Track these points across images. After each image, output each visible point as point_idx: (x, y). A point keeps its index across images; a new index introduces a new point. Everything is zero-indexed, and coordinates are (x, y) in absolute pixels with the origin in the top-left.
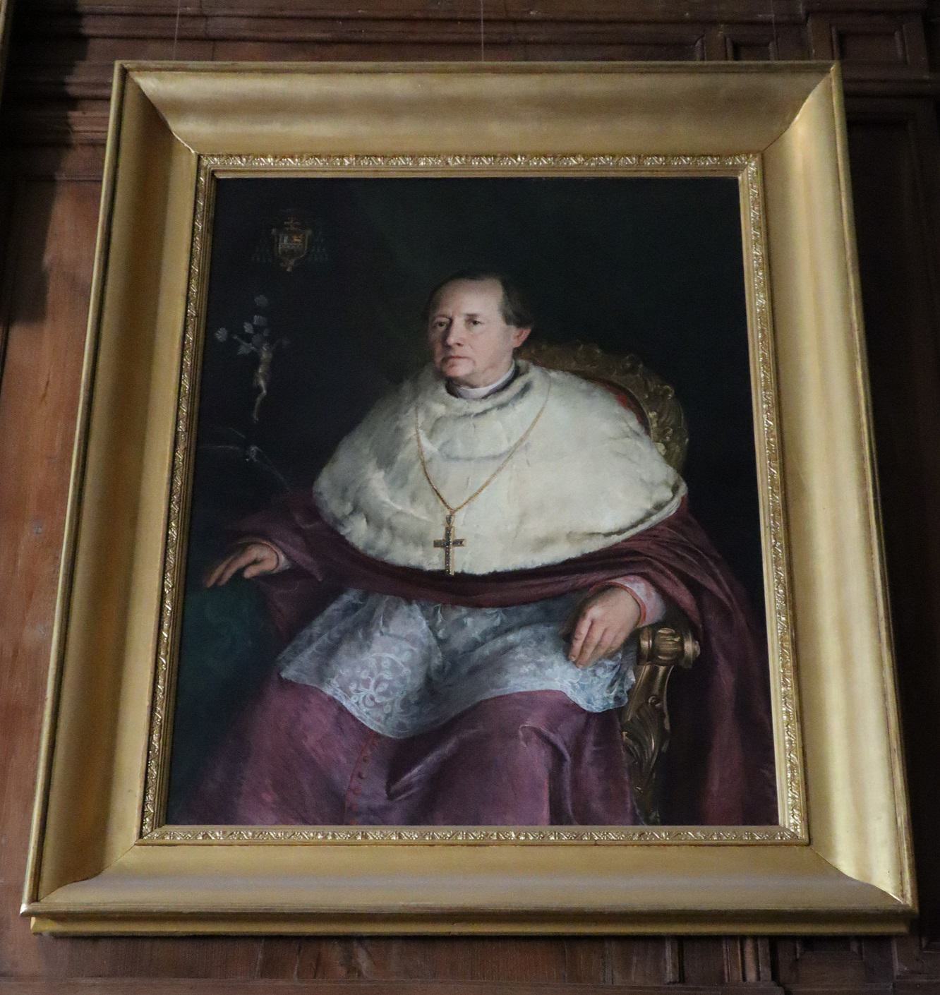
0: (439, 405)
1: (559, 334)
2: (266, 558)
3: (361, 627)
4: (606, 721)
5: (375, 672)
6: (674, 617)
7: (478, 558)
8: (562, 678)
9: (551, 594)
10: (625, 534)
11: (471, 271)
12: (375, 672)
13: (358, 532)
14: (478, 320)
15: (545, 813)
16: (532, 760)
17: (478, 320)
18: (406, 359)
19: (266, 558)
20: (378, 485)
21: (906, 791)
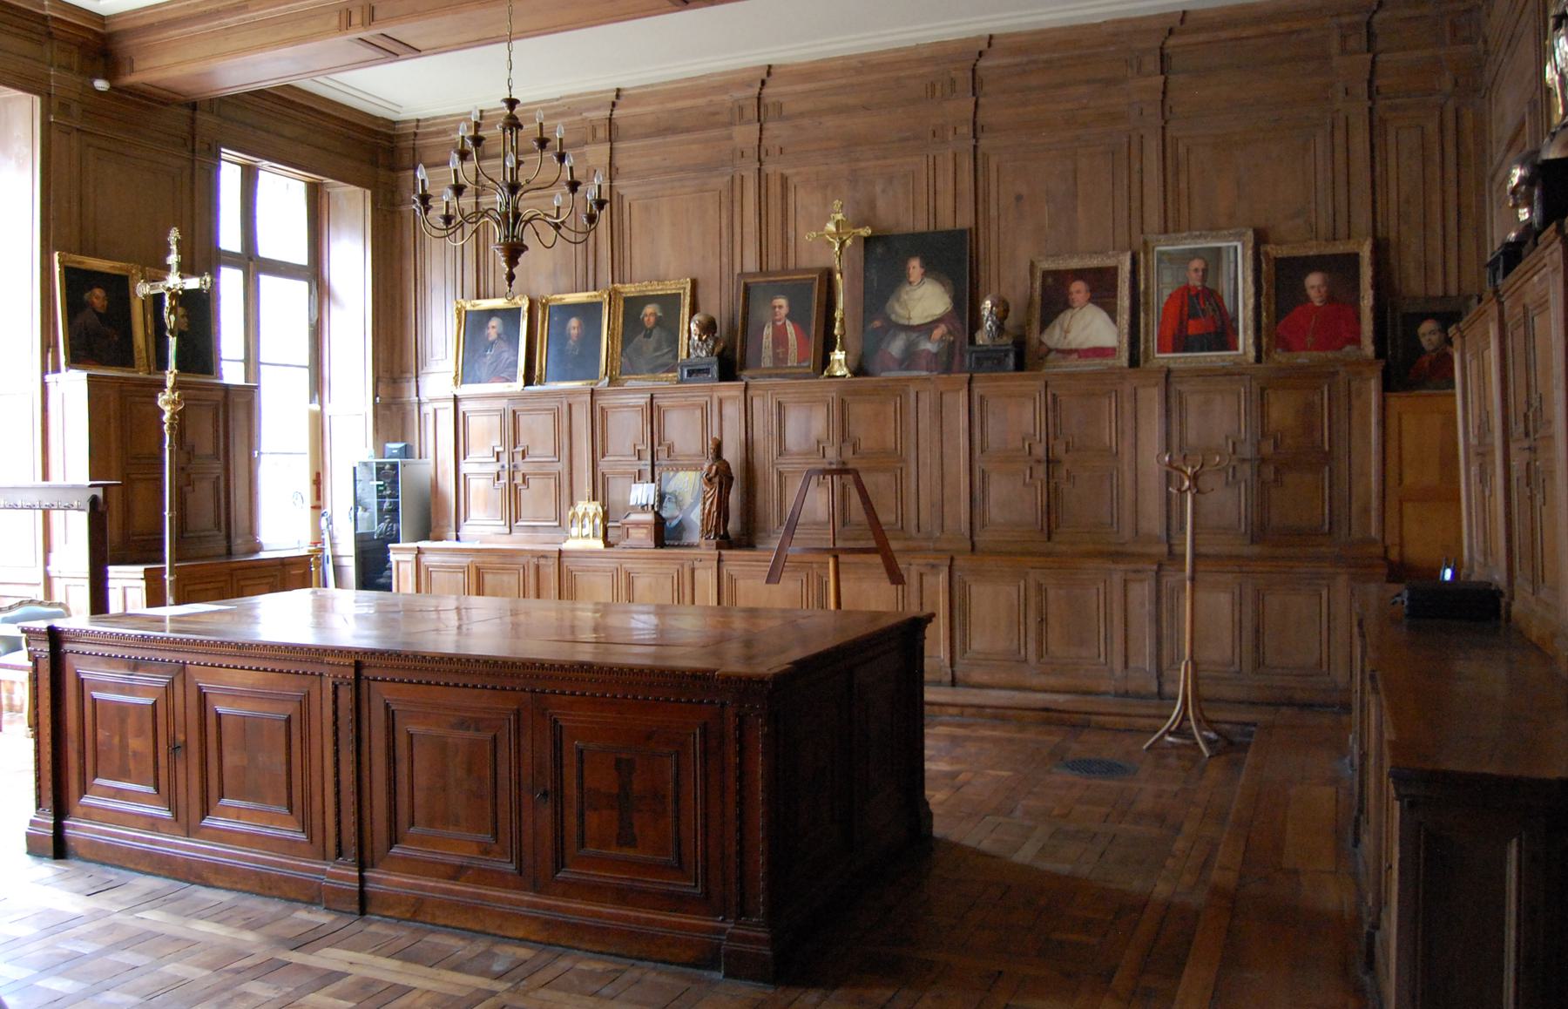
0: (908, 288)
1: (932, 269)
2: (877, 324)
3: (895, 336)
4: (936, 355)
5: (896, 347)
6: (950, 332)
7: (916, 321)
8: (929, 346)
9: (926, 329)
10: (602, 81)
11: (912, 255)
12: (896, 347)
13: (893, 317)
14: (915, 267)
15: (51, 853)
16: (923, 362)
17: (915, 267)
18: (899, 278)
19: (877, 324)
20: (897, 307)
21: (823, 60)
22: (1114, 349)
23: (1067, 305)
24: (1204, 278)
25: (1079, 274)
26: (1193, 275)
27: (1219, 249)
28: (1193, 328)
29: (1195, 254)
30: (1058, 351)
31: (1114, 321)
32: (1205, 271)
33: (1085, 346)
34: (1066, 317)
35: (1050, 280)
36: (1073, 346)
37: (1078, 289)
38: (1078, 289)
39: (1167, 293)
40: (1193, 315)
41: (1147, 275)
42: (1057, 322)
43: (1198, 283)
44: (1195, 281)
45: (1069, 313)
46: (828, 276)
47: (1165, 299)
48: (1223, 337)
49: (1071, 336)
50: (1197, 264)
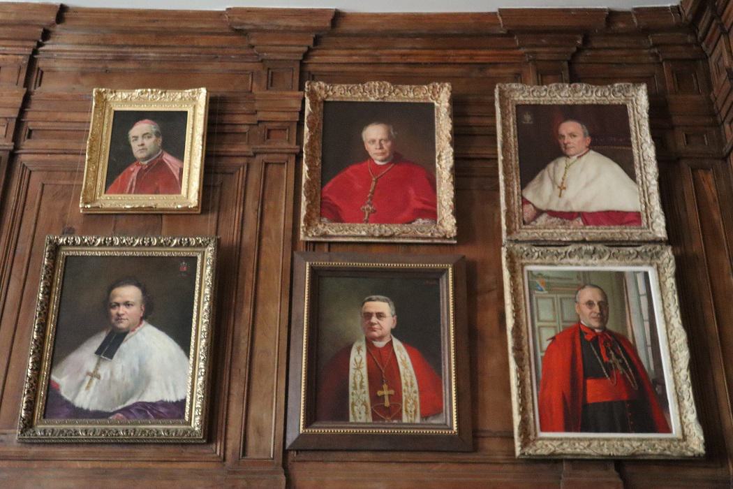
22: (638, 215)
23: (556, 151)
24: (603, 317)
25: (571, 112)
26: (586, 310)
27: (620, 276)
28: (595, 391)
29: (585, 279)
30: (552, 214)
31: (632, 176)
32: (603, 305)
33: (593, 208)
34: (558, 167)
35: (528, 118)
36: (575, 207)
37: (572, 133)
38: (572, 133)
39: (547, 335)
40: (593, 371)
41: (516, 304)
42: (547, 173)
43: (595, 324)
44: (589, 319)
45: (562, 162)
46: (105, 193)
47: (546, 344)
48: (645, 409)
49: (569, 194)
50: (588, 294)
